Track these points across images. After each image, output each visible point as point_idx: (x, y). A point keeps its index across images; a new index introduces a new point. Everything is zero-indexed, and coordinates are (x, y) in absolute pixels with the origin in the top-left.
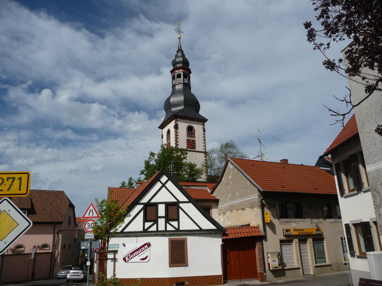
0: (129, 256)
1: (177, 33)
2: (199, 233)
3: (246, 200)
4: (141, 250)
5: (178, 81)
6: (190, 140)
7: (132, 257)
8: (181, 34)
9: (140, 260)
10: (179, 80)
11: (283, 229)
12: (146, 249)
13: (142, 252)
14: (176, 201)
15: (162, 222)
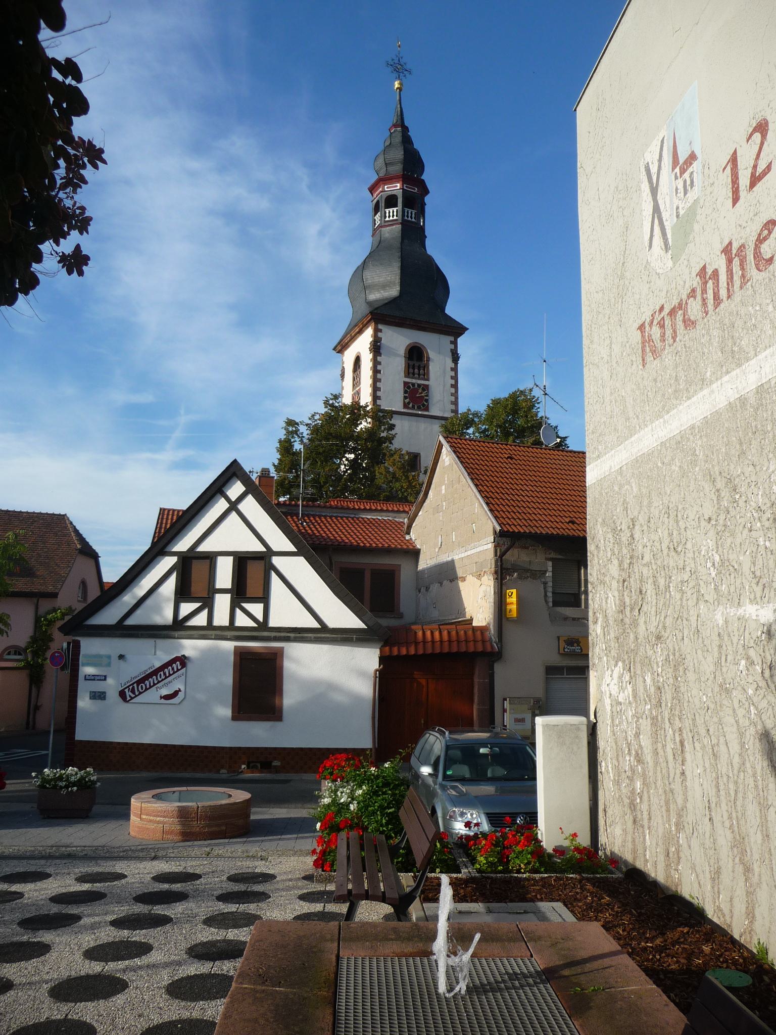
0: (133, 688)
1: (392, 72)
2: (315, 637)
3: (469, 553)
4: (165, 674)
5: (389, 217)
6: (413, 384)
7: (142, 689)
8: (405, 76)
9: (161, 698)
10: (391, 214)
11: (558, 638)
12: (176, 672)
13: (166, 678)
14: (264, 550)
15: (222, 603)
